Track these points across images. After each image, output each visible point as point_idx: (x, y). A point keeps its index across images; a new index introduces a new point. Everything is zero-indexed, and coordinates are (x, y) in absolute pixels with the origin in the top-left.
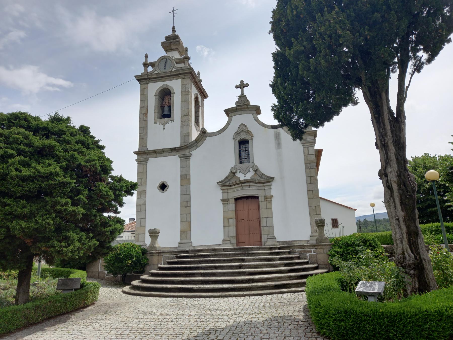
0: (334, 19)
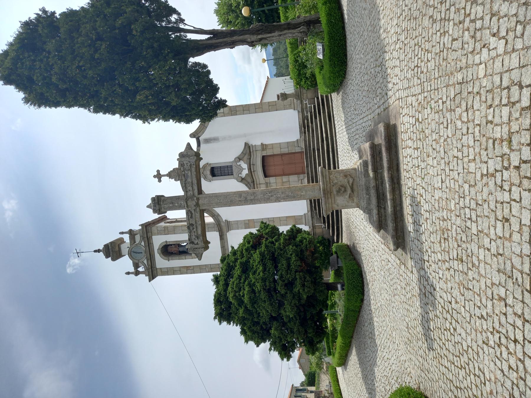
0: (158, 71)
